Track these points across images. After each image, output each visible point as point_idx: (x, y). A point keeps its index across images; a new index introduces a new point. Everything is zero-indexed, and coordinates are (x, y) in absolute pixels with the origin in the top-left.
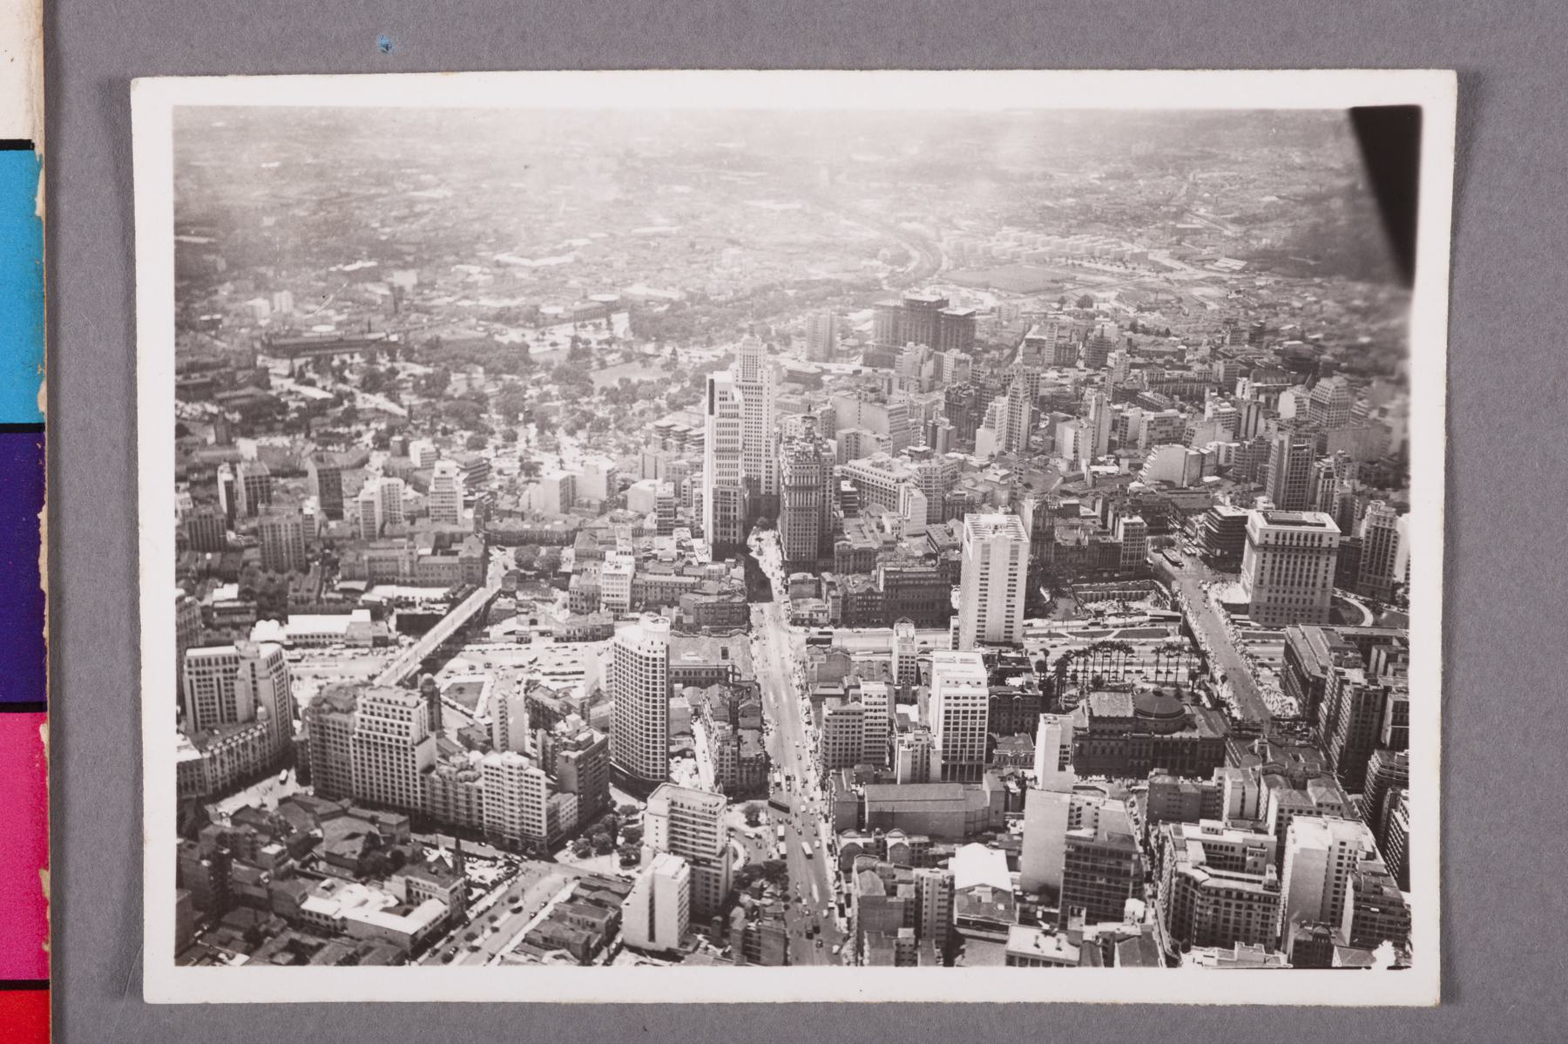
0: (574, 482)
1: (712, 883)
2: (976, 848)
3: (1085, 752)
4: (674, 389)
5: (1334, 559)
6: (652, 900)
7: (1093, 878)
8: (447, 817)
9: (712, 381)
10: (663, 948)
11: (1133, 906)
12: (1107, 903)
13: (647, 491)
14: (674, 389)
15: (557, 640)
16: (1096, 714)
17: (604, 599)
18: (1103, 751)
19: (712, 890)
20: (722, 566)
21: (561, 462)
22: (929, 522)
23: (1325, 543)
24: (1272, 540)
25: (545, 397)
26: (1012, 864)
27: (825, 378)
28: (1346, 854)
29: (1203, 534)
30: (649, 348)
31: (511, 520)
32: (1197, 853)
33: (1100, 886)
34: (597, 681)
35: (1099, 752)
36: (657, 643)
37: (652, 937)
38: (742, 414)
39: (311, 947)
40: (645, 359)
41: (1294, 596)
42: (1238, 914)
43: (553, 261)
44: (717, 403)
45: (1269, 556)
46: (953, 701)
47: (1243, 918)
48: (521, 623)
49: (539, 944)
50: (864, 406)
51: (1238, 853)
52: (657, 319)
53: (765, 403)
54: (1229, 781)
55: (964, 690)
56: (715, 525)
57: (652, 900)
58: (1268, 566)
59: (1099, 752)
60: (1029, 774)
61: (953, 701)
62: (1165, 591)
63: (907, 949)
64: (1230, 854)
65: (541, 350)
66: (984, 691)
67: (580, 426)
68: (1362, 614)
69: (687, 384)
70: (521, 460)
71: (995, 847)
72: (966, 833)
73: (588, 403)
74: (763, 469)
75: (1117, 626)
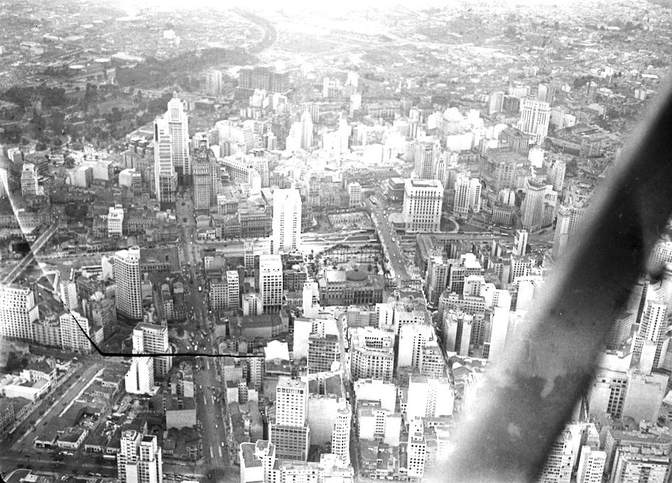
0: (92, 171)
1: (163, 364)
2: (276, 342)
3: (326, 297)
4: (140, 114)
5: (441, 202)
6: (137, 373)
7: (320, 354)
8: (45, 342)
9: (156, 125)
10: (143, 393)
11: (335, 365)
12: (326, 363)
13: (126, 177)
14: (140, 114)
15: (88, 252)
16: (330, 281)
17: (110, 231)
18: (337, 296)
19: (163, 370)
20: (165, 214)
21: (85, 156)
22: (262, 187)
23: (437, 195)
24: (414, 194)
25: (75, 119)
26: (290, 348)
27: (217, 106)
28: (421, 342)
29: (387, 189)
30: (127, 90)
31: (90, 373)
32: (363, 341)
33: (323, 357)
34: (108, 274)
35: (331, 297)
36: (134, 258)
37: (138, 389)
38: (171, 141)
39: (310, 430)
40: (125, 95)
41: (422, 219)
42: (378, 365)
43: (75, 38)
44: (159, 136)
45: (413, 201)
46: (267, 278)
47: (380, 366)
48: (70, 244)
49: (53, 282)
50: (232, 128)
51: (380, 340)
52: (130, 72)
53: (183, 131)
54: (384, 309)
55: (274, 274)
56: (161, 193)
57: (137, 373)
58: (413, 205)
59: (331, 297)
60: (300, 309)
61: (267, 278)
62: (369, 217)
63: (243, 390)
64: (376, 340)
65: (71, 91)
66: (281, 273)
67: (94, 136)
68: (455, 226)
69: (146, 111)
70: (65, 156)
71: (283, 342)
72: (273, 336)
73: (97, 122)
74: (184, 162)
75: (347, 235)
